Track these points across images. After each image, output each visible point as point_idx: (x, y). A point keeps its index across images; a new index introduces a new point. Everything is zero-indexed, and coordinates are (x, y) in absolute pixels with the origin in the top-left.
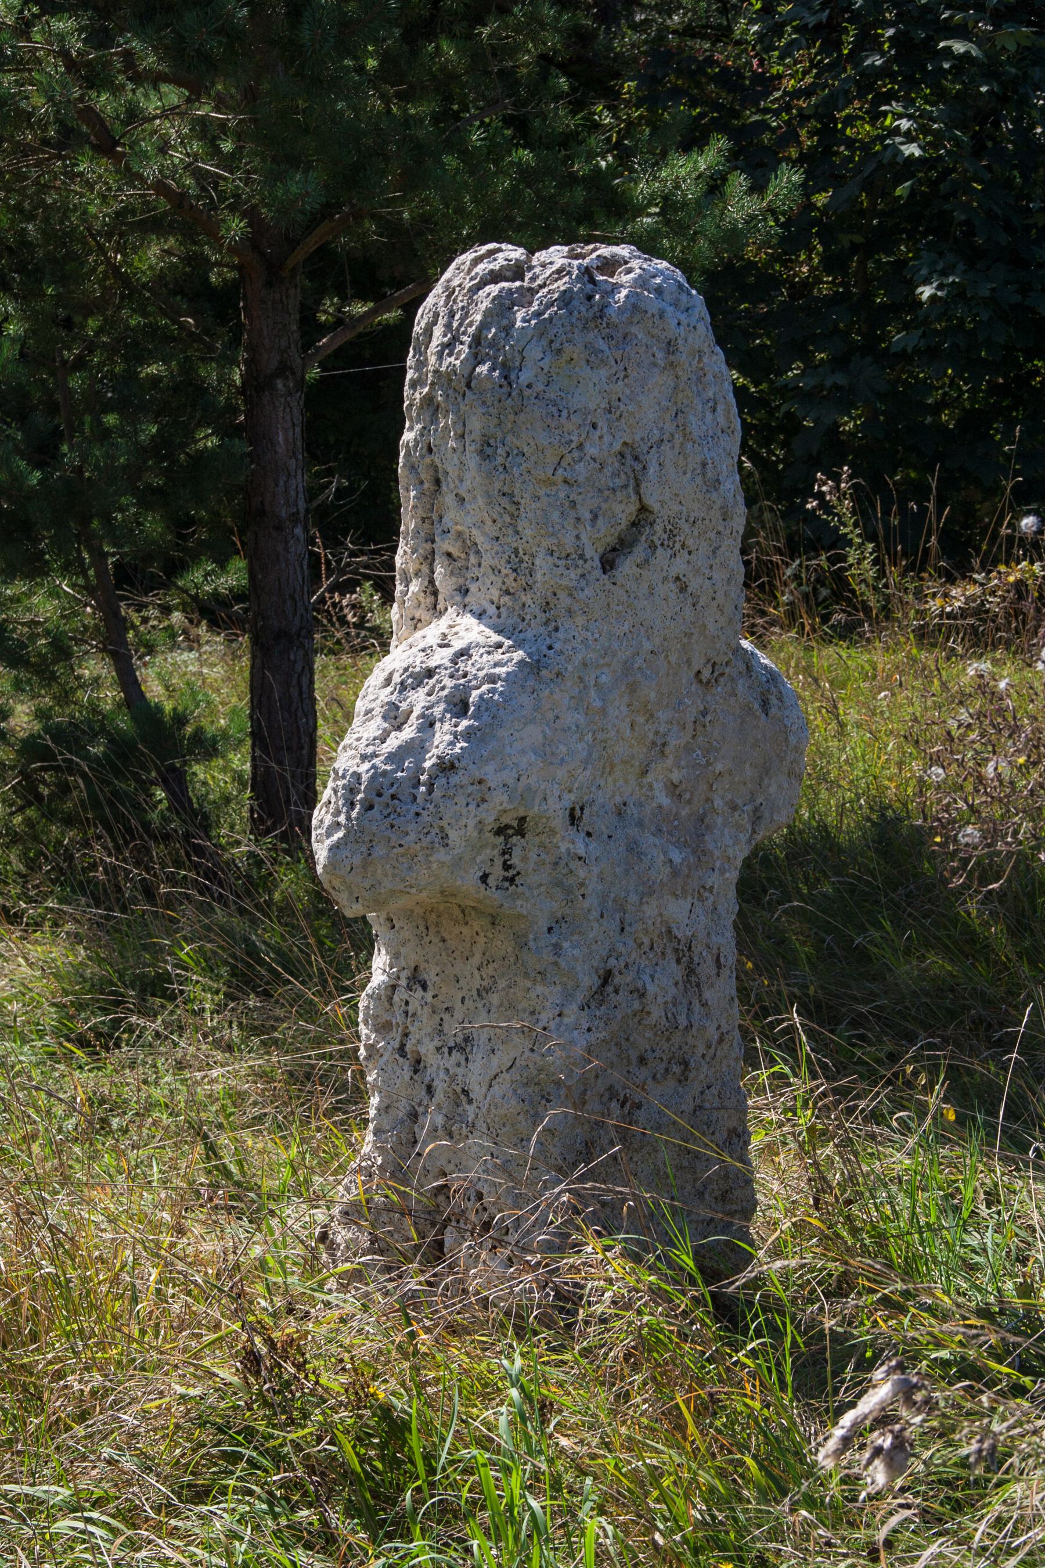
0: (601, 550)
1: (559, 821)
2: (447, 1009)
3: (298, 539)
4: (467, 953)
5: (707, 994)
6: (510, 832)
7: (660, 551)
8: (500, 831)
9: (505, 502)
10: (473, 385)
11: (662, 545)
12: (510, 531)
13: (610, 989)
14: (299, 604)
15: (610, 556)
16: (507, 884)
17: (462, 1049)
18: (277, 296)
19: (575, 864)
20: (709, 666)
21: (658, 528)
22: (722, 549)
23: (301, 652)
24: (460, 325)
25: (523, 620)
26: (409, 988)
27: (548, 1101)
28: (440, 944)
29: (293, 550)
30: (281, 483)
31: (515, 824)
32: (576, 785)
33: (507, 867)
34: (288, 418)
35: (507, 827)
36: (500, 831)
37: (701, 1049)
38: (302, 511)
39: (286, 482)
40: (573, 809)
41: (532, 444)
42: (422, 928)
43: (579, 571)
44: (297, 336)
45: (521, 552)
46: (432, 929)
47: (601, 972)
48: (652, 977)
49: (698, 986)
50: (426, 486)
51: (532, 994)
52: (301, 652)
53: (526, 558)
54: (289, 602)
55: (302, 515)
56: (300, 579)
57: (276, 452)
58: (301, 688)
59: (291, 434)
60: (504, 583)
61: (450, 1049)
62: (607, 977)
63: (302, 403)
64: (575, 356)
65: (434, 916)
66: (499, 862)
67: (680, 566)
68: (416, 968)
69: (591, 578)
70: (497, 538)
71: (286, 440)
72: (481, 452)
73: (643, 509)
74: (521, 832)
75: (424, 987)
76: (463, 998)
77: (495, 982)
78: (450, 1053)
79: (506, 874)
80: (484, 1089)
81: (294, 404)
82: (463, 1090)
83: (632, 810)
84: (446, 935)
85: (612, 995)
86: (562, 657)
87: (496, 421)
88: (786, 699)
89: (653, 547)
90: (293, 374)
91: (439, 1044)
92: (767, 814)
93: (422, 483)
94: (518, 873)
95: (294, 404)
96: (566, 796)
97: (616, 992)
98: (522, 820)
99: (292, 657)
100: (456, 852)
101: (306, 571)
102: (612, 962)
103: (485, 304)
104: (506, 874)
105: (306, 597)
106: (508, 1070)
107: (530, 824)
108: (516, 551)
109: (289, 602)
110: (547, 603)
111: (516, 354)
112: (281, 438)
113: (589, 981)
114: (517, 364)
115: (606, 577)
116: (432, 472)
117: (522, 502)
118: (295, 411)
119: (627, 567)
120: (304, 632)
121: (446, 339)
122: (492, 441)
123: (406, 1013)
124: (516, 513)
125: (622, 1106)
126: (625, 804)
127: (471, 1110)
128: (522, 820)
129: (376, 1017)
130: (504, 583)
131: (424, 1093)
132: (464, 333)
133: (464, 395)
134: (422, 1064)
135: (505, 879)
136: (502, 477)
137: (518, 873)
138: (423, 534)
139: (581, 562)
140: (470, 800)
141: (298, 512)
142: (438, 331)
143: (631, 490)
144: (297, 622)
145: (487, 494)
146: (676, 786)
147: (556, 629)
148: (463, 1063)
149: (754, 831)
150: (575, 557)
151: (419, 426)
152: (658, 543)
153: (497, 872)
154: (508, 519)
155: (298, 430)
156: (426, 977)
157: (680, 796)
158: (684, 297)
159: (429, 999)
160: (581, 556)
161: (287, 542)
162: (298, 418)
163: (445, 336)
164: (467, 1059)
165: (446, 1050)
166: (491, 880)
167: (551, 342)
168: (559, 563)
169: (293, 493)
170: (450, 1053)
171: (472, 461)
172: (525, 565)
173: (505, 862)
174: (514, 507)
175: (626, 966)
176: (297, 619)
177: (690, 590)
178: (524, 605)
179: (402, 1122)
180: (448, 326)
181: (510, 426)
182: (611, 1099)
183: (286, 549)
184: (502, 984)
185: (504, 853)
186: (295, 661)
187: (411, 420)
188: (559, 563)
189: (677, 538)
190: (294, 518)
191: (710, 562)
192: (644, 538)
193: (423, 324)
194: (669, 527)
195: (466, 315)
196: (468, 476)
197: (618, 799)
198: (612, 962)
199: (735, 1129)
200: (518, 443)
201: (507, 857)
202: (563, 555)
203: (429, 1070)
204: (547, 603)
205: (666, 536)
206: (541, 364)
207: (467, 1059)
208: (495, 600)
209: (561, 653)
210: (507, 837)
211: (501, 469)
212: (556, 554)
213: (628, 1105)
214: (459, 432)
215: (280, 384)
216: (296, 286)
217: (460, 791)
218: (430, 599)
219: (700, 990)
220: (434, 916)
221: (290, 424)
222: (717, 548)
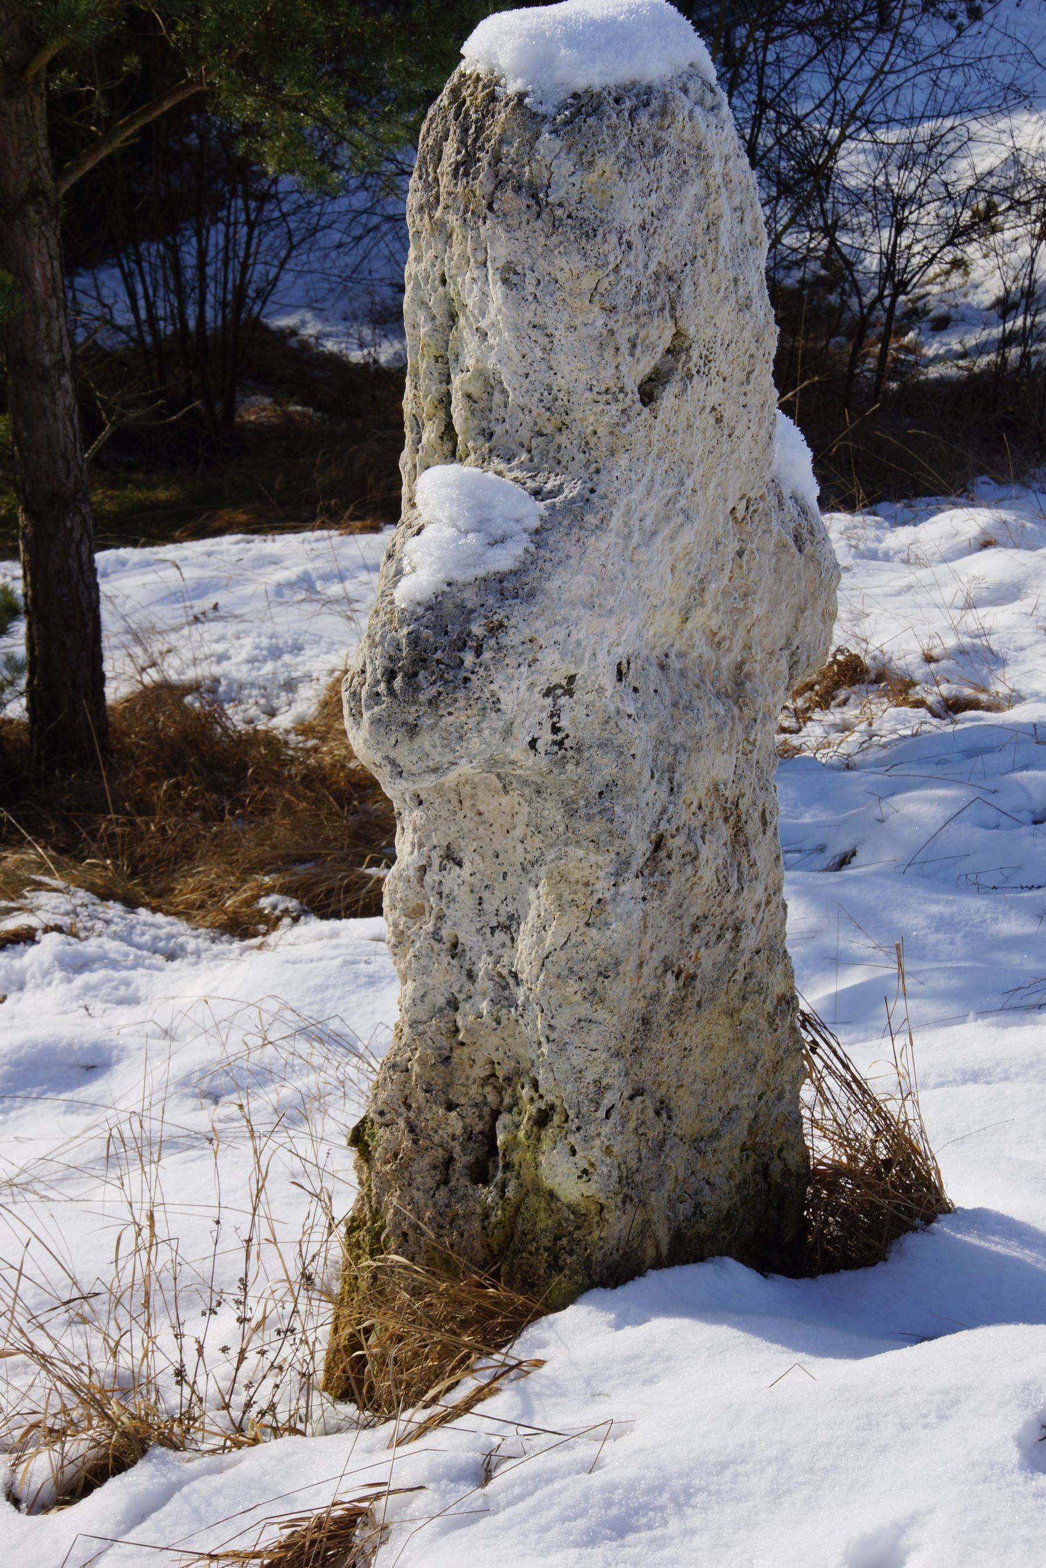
0: (638, 382)
1: (608, 679)
2: (487, 887)
3: (66, 391)
4: (507, 826)
5: (754, 852)
6: (559, 692)
7: (696, 378)
8: (548, 693)
9: (536, 334)
10: (495, 207)
11: (698, 372)
12: (543, 366)
13: (663, 854)
14: (72, 463)
15: (647, 388)
16: (556, 748)
17: (507, 928)
18: (21, 107)
19: (624, 723)
20: (744, 502)
21: (695, 354)
22: (755, 373)
23: (78, 519)
24: (476, 140)
25: (559, 463)
26: (442, 868)
27: (607, 977)
28: (477, 818)
29: (60, 402)
30: (43, 326)
31: (564, 682)
32: (624, 638)
33: (555, 730)
34: (45, 250)
35: (556, 687)
36: (548, 693)
37: (750, 912)
38: (68, 357)
39: (48, 325)
40: (620, 664)
41: (566, 269)
42: (455, 801)
43: (620, 406)
44: (46, 154)
45: (555, 388)
46: (467, 803)
47: (653, 836)
48: (703, 838)
49: (746, 845)
50: (438, 322)
51: (585, 864)
52: (78, 519)
53: (560, 395)
54: (61, 463)
55: (68, 362)
56: (71, 436)
57: (33, 291)
58: (80, 558)
59: (48, 267)
60: (536, 424)
61: (493, 930)
62: (658, 844)
63: (58, 232)
64: (607, 168)
65: (468, 787)
66: (547, 725)
67: (714, 397)
68: (448, 847)
69: (632, 413)
70: (527, 375)
71: (44, 276)
72: (505, 281)
73: (678, 334)
74: (570, 693)
75: (460, 864)
76: (505, 874)
77: (542, 854)
78: (492, 934)
79: (555, 737)
80: (535, 970)
81: (49, 234)
82: (511, 972)
83: (675, 664)
84: (482, 808)
85: (665, 861)
86: (606, 501)
87: (524, 246)
88: (816, 533)
89: (690, 377)
90: (46, 198)
91: (479, 925)
92: (803, 658)
93: (434, 318)
94: (567, 736)
95: (49, 234)
96: (614, 650)
97: (669, 857)
98: (571, 679)
99: (69, 524)
100: (508, 717)
101: (77, 426)
102: (663, 826)
103: (503, 115)
104: (555, 737)
105: (79, 454)
106: (562, 948)
107: (579, 682)
108: (549, 388)
109: (61, 463)
110: (587, 443)
111: (544, 170)
112: (38, 274)
113: (643, 848)
114: (545, 181)
115: (646, 410)
116: (445, 306)
117: (557, 333)
118: (53, 243)
119: (668, 398)
120: (79, 496)
121: (459, 157)
122: (519, 269)
123: (440, 894)
124: (549, 347)
125: (677, 978)
126: (666, 656)
127: (521, 994)
128: (571, 679)
129: (405, 900)
130: (536, 424)
131: (464, 978)
132: (481, 149)
133: (485, 218)
134: (460, 948)
135: (554, 743)
136: (533, 307)
137: (567, 736)
138: (436, 375)
139: (621, 396)
140: (521, 660)
141: (64, 359)
142: (450, 148)
143: (667, 313)
144: (71, 484)
145: (516, 328)
146: (715, 634)
147: (598, 471)
148: (509, 943)
149: (791, 677)
150: (612, 394)
151: (431, 253)
152: (694, 371)
153: (546, 737)
154: (539, 354)
155: (56, 264)
156: (462, 855)
157: (719, 644)
158: (709, 96)
159: (467, 878)
160: (622, 390)
161: (53, 395)
162: (55, 250)
163: (459, 152)
164: (512, 939)
165: (488, 931)
166: (539, 745)
167: (582, 154)
168: (599, 398)
169: (56, 338)
170: (492, 934)
171: (496, 291)
172: (559, 403)
173: (553, 725)
174: (547, 340)
175: (677, 829)
176: (72, 480)
177: (725, 421)
178: (559, 447)
179: (441, 1010)
180: (462, 142)
181: (540, 250)
182: (665, 971)
183: (54, 401)
184: (550, 856)
185: (552, 716)
186: (72, 529)
187: (418, 248)
188: (599, 398)
189: (712, 364)
190: (60, 366)
191: (744, 390)
192: (680, 365)
193: (430, 141)
194: (704, 352)
195: (480, 130)
196: (493, 308)
197: (658, 652)
198: (663, 826)
199: (784, 996)
200: (550, 269)
201: (555, 719)
202: (603, 389)
203: (468, 954)
204: (587, 443)
205: (702, 363)
206: (571, 180)
207: (512, 939)
208: (526, 443)
209: (604, 497)
210: (556, 698)
211: (531, 298)
212: (596, 390)
213: (683, 975)
214: (481, 258)
215: (31, 210)
216: (41, 95)
217: (511, 651)
218: (448, 446)
219: (748, 851)
220: (468, 787)
221: (47, 257)
222: (750, 372)
